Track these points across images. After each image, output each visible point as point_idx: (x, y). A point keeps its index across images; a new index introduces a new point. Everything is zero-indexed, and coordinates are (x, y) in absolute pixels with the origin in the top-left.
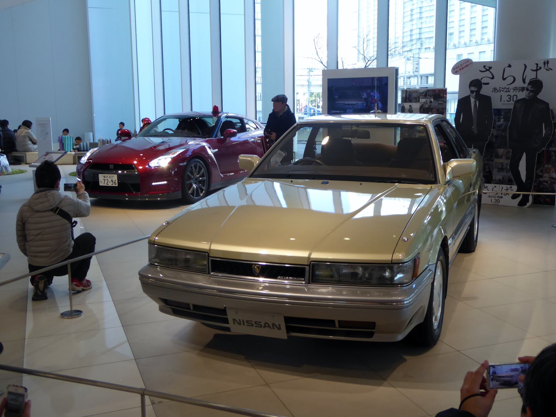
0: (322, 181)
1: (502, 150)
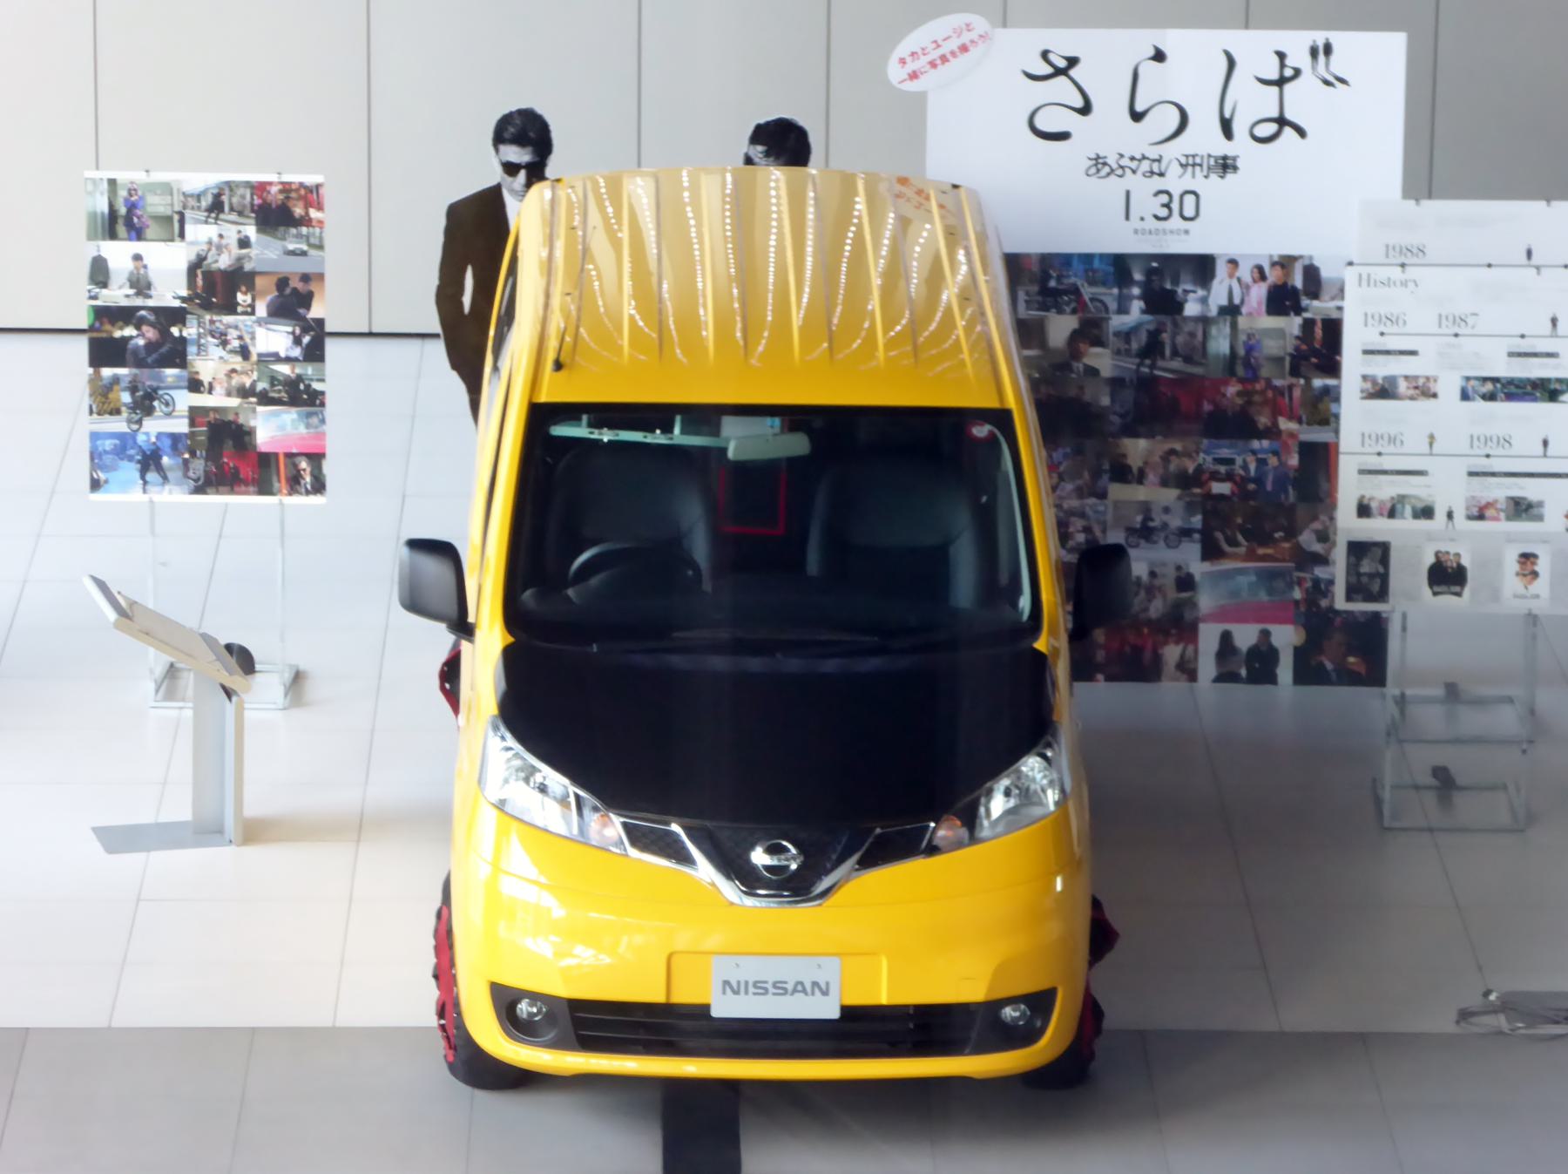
1: (1142, 443)
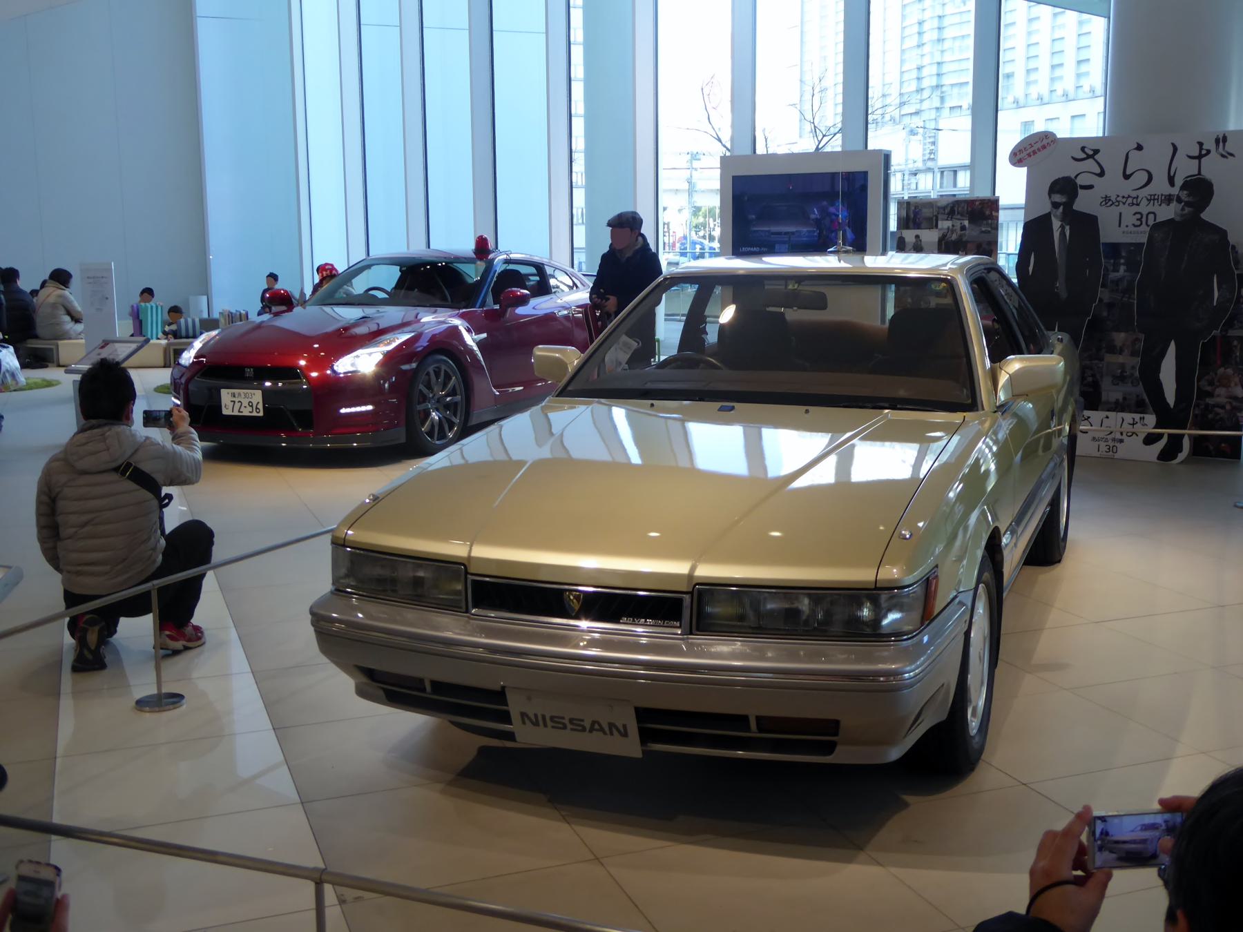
0: (719, 404)
1: (1123, 335)
